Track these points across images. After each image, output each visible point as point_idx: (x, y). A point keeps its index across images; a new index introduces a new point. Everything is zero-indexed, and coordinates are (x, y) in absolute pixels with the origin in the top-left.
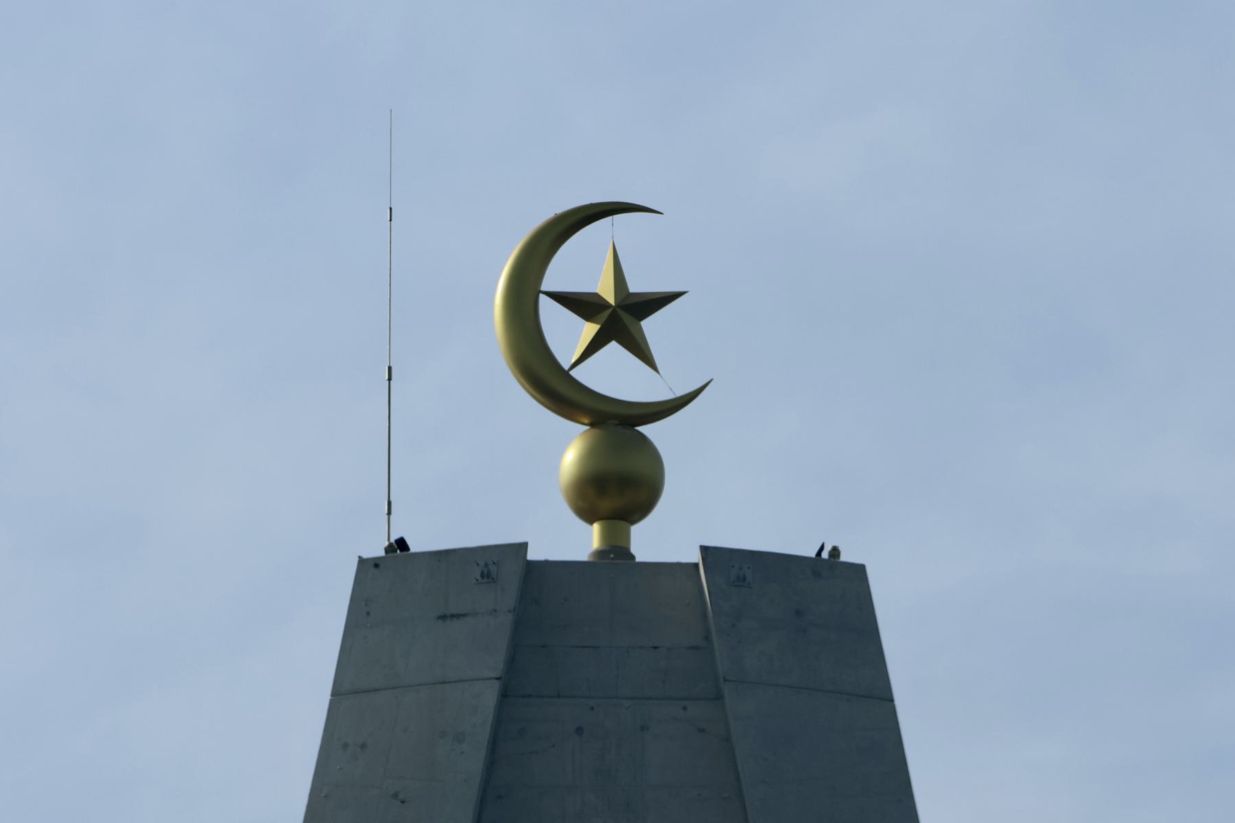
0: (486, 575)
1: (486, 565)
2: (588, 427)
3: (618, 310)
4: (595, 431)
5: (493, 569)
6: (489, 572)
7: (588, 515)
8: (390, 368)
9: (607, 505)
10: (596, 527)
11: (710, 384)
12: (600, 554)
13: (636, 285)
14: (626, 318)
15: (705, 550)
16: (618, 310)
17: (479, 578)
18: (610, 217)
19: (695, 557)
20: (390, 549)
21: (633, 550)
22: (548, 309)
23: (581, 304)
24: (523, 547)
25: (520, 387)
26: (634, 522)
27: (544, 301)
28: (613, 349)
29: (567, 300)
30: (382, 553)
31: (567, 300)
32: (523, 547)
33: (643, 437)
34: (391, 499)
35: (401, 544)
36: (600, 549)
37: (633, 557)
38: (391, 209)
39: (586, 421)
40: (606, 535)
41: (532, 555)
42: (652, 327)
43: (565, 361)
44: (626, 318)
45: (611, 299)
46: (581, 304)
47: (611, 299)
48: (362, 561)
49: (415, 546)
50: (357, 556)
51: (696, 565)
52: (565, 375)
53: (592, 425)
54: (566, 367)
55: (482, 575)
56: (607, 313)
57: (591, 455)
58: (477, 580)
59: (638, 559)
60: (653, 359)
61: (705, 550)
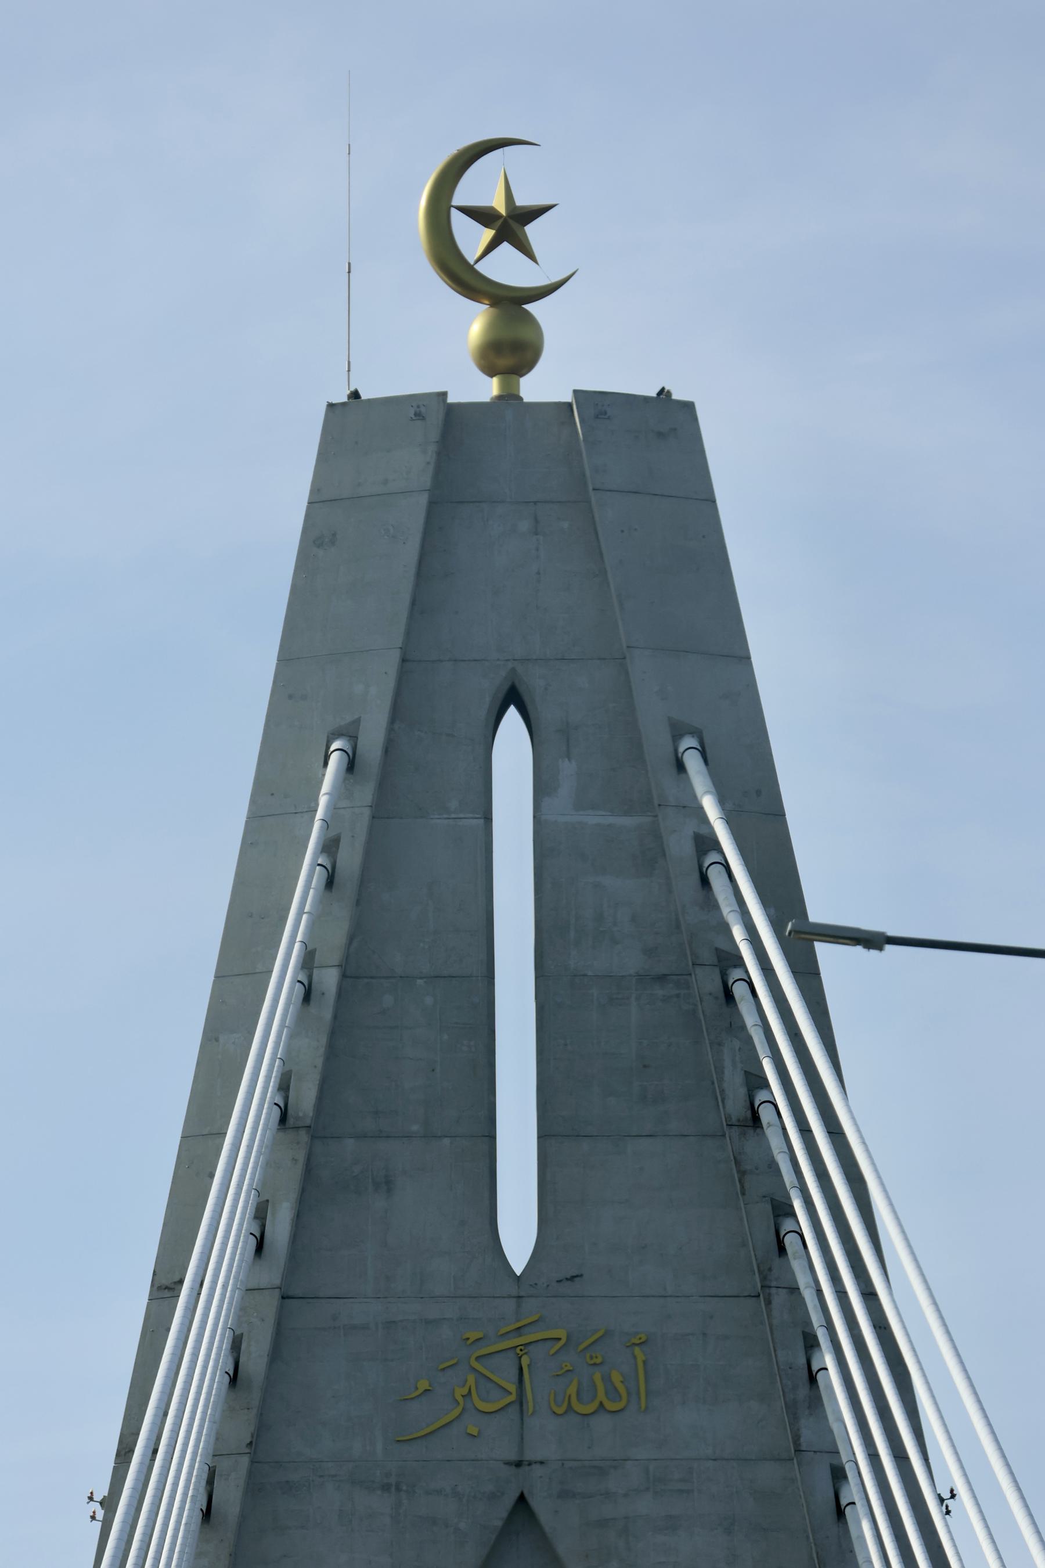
0: (419, 415)
1: (418, 407)
2: (489, 306)
3: (510, 221)
4: (492, 309)
5: (423, 409)
6: (420, 411)
7: (490, 371)
8: (349, 264)
9: (504, 362)
10: (495, 381)
11: (576, 274)
12: (499, 398)
13: (522, 200)
14: (514, 225)
15: (575, 392)
16: (510, 221)
17: (413, 416)
18: (502, 149)
19: (568, 397)
20: (349, 397)
21: (522, 394)
22: (457, 217)
23: (482, 215)
24: (444, 395)
25: (439, 279)
26: (522, 375)
27: (454, 211)
28: (506, 248)
29: (470, 212)
30: (345, 399)
31: (470, 212)
32: (444, 395)
33: (523, 308)
34: (350, 360)
35: (355, 395)
36: (759, 1090)
37: (521, 399)
38: (349, 145)
39: (487, 302)
40: (503, 385)
41: (451, 399)
42: (533, 231)
43: (471, 259)
44: (514, 225)
45: (503, 211)
46: (482, 215)
47: (503, 211)
48: (331, 406)
49: (364, 396)
50: (87, 1498)
51: (570, 405)
52: (471, 268)
53: (492, 305)
54: (472, 263)
55: (415, 415)
56: (499, 223)
57: (492, 326)
58: (411, 418)
59: (525, 400)
60: (533, 253)
61: (575, 392)
